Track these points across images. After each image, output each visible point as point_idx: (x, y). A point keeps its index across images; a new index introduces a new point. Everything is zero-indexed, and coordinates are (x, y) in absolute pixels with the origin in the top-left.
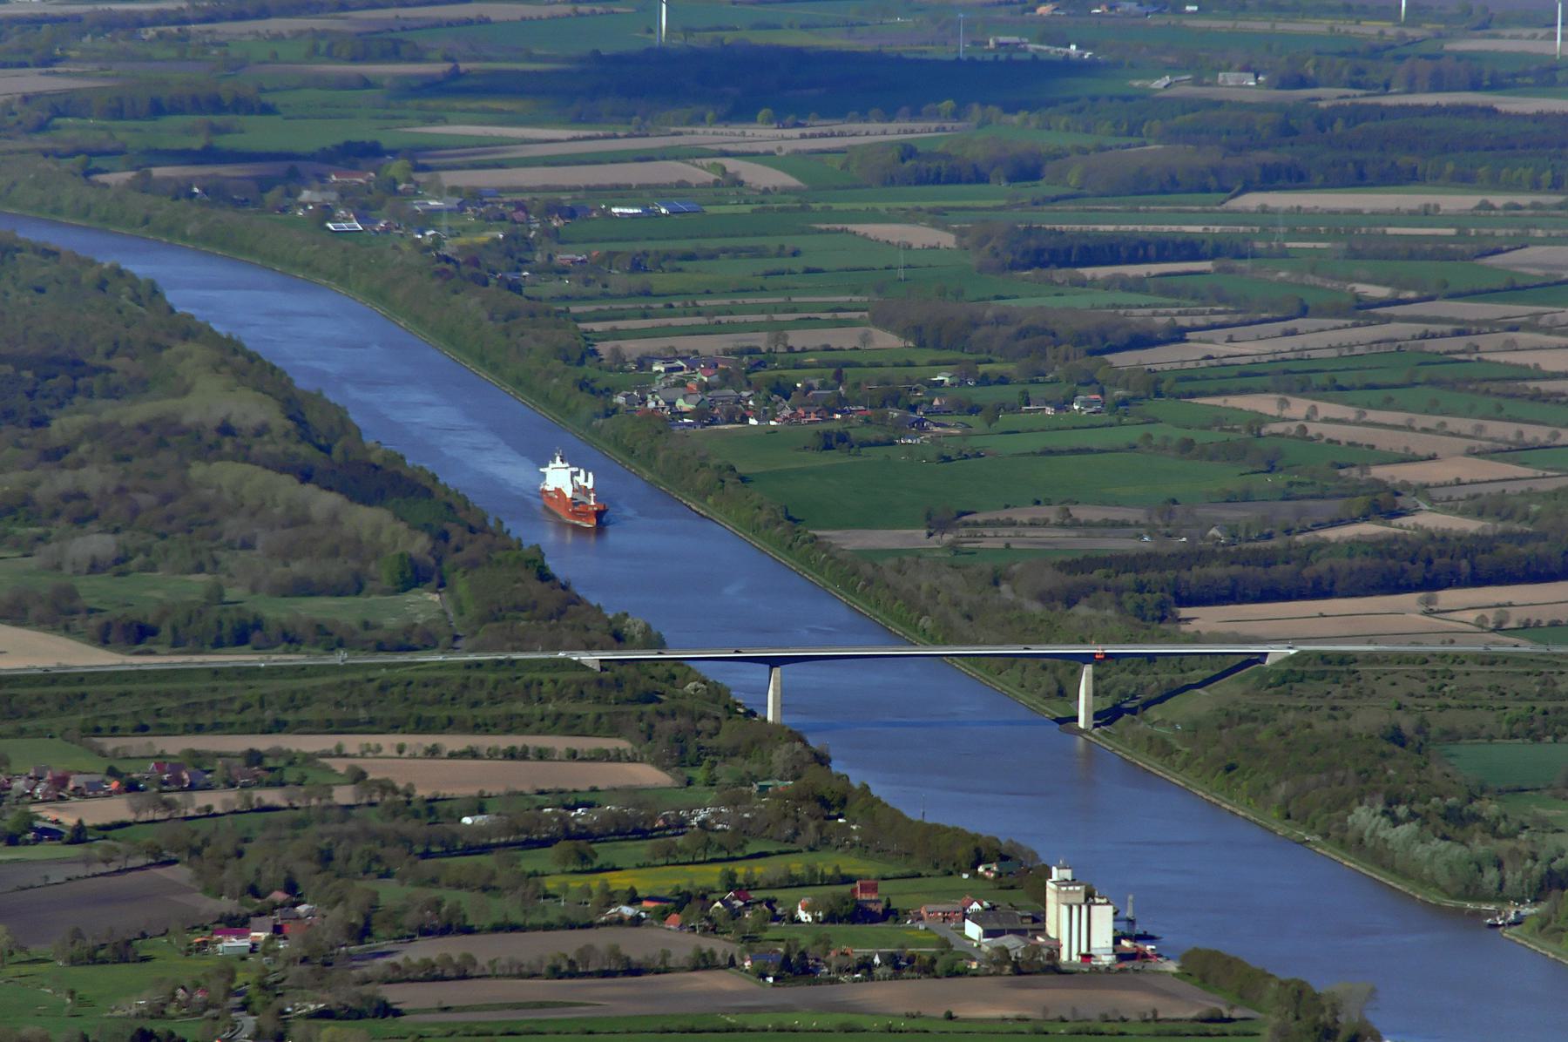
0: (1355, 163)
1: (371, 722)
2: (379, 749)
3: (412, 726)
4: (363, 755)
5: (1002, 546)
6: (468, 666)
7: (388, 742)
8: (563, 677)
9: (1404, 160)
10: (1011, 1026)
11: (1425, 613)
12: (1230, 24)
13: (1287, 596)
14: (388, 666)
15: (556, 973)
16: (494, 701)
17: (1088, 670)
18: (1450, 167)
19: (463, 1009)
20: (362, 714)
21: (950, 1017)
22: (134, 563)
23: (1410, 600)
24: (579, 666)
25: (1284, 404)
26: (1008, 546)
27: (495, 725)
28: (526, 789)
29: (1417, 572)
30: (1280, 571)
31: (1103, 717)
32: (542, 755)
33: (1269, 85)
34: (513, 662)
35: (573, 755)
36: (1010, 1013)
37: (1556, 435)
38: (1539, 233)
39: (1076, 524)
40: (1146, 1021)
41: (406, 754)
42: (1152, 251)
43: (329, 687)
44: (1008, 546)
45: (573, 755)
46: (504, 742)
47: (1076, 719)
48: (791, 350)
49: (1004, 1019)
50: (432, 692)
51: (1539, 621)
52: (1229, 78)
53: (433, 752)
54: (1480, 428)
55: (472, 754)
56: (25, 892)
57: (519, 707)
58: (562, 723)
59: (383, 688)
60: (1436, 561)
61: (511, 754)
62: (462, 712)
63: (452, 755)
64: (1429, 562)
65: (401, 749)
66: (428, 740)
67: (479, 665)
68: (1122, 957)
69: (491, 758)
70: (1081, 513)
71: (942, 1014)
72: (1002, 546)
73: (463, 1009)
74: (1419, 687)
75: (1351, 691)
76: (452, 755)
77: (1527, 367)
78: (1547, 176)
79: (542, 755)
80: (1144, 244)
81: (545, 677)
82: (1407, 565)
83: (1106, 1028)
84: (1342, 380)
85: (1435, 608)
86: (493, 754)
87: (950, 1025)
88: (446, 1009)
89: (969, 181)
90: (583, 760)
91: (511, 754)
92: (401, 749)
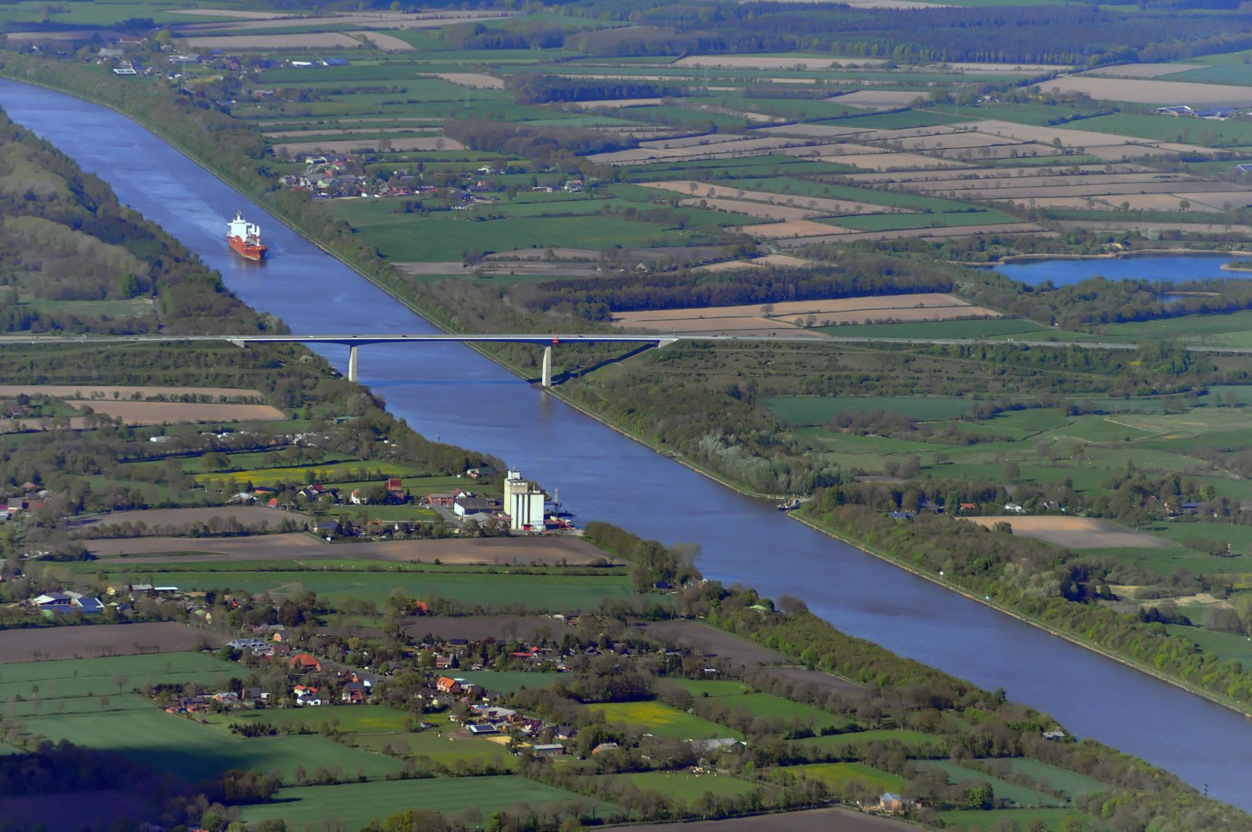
1: (100, 378)
2: (103, 395)
3: (125, 381)
4: (93, 399)
5: (509, 273)
6: (162, 344)
7: (108, 391)
9: (787, 37)
10: (475, 569)
11: (766, 317)
15: (196, 534)
19: (135, 556)
20: (95, 373)
21: (438, 563)
23: (757, 308)
24: (231, 344)
25: (694, 187)
26: (512, 273)
27: (177, 381)
28: (193, 420)
29: (762, 291)
31: (558, 379)
32: (205, 399)
34: (190, 342)
35: (224, 400)
36: (475, 561)
37: (860, 208)
38: (867, 83)
40: (560, 566)
41: (119, 398)
42: (625, 92)
43: (74, 357)
44: (512, 273)
45: (224, 400)
46: (181, 391)
47: (541, 380)
48: (393, 151)
49: (471, 565)
50: (138, 360)
51: (835, 323)
53: (137, 397)
54: (813, 203)
55: (161, 398)
57: (193, 370)
59: (108, 357)
61: (186, 399)
63: (149, 399)
65: (116, 395)
66: (134, 390)
67: (168, 343)
68: (549, 527)
69: (173, 401)
70: (559, 253)
71: (433, 561)
72: (509, 273)
73: (135, 556)
74: (754, 363)
75: (710, 364)
76: (149, 399)
77: (848, 165)
78: (875, 48)
79: (205, 399)
80: (620, 87)
81: (210, 351)
85: (772, 314)
86: (174, 399)
88: (125, 556)
90: (231, 403)
91: (186, 399)
92: (116, 395)
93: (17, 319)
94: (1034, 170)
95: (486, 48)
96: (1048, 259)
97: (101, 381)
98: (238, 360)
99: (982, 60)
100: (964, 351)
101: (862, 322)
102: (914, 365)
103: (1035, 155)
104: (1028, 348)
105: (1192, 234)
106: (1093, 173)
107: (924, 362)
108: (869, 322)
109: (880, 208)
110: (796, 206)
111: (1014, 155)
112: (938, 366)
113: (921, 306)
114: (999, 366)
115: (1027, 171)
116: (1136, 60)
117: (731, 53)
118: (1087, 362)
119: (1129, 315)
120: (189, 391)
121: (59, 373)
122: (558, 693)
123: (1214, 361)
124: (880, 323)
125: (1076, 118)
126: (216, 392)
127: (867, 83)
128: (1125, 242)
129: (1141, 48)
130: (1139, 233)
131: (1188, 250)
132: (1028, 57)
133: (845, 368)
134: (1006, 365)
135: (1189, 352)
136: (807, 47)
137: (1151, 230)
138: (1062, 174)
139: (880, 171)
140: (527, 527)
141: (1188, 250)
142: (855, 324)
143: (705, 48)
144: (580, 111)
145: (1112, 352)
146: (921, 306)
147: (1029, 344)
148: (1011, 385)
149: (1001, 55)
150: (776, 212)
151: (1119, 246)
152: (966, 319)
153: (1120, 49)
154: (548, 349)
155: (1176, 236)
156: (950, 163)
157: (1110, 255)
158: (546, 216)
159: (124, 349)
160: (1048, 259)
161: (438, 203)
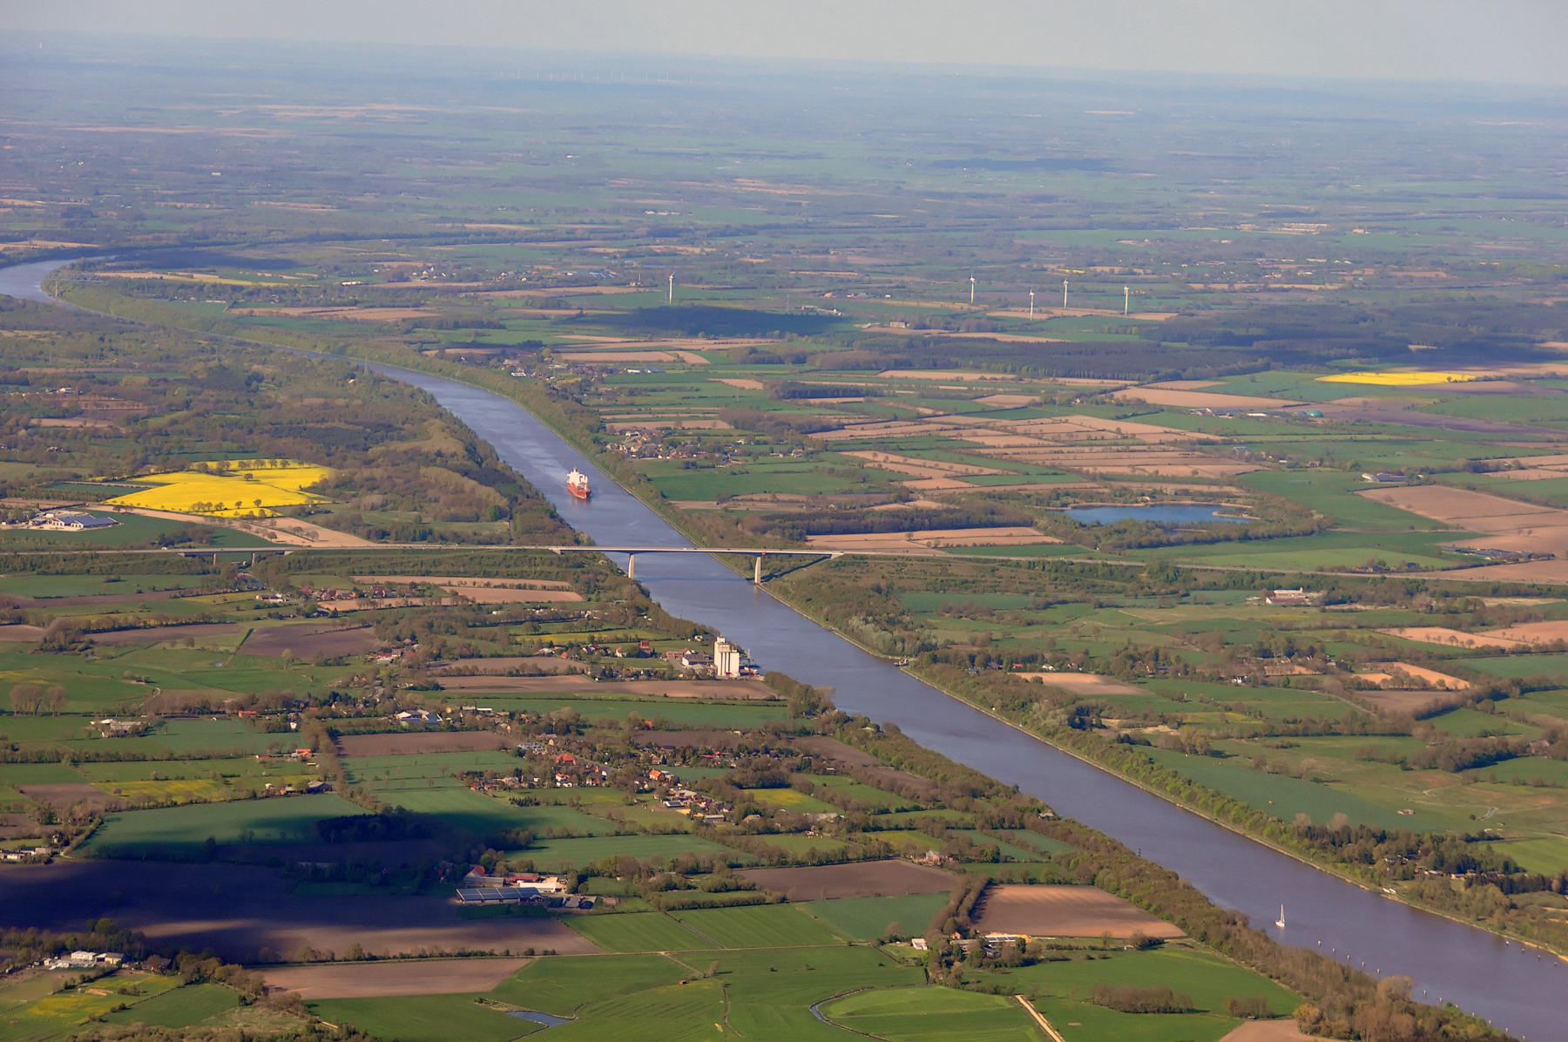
1: (465, 572)
8: (544, 556)
9: (954, 359)
10: (689, 700)
17: (759, 559)
19: (469, 688)
21: (665, 696)
24: (552, 552)
29: (907, 524)
31: (765, 579)
32: (532, 588)
35: (544, 588)
36: (690, 695)
38: (1001, 390)
42: (841, 393)
43: (449, 558)
45: (544, 588)
46: (516, 582)
48: (683, 428)
52: (895, 324)
53: (488, 585)
54: (951, 467)
55: (504, 586)
57: (526, 568)
58: (543, 575)
61: (519, 587)
63: (495, 587)
66: (486, 580)
67: (511, 551)
68: (742, 674)
70: (780, 497)
73: (469, 688)
74: (893, 570)
76: (495, 587)
78: (1009, 368)
79: (532, 588)
81: (537, 556)
87: (665, 699)
91: (519, 587)
92: (474, 583)
93: (418, 534)
95: (756, 363)
97: (466, 574)
100: (1031, 565)
101: (970, 545)
102: (997, 573)
103: (1103, 438)
104: (1072, 564)
105: (1196, 492)
107: (1003, 571)
108: (975, 545)
109: (995, 471)
111: (1089, 438)
113: (1011, 535)
114: (1053, 575)
115: (1095, 449)
118: (1111, 573)
120: (522, 582)
123: (1194, 574)
124: (982, 546)
125: (1134, 415)
127: (1001, 390)
129: (1184, 370)
130: (1161, 491)
133: (953, 575)
137: (1170, 489)
142: (966, 546)
147: (1074, 561)
148: (1060, 588)
149: (1091, 373)
153: (1170, 371)
155: (1186, 493)
156: (1046, 443)
159: (483, 554)
160: (1101, 506)
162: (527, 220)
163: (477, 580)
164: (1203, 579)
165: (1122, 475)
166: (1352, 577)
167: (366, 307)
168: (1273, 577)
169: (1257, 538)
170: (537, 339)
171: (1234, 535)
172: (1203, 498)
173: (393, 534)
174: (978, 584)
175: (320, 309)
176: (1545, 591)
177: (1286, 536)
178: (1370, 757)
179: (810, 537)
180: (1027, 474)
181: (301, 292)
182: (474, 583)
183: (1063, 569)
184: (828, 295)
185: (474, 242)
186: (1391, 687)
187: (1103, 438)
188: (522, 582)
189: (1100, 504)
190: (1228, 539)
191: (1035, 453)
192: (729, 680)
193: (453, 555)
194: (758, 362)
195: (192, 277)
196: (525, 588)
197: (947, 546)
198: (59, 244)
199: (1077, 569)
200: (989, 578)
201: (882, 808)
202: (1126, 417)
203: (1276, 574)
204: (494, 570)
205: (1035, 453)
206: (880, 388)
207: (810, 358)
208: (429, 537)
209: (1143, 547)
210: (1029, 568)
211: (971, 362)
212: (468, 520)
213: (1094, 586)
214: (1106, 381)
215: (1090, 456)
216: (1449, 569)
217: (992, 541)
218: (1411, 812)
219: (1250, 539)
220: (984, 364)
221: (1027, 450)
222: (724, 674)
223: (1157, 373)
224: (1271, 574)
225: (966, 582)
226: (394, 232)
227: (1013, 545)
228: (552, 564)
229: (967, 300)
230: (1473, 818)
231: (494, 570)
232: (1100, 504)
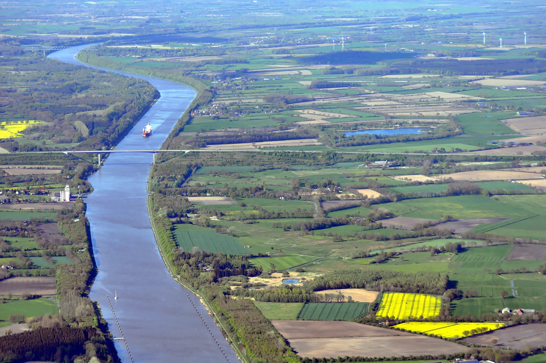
0: (409, 70)
1: (22, 163)
6: (44, 154)
8: (58, 155)
9: (418, 69)
12: (465, 46)
13: (234, 143)
14: (30, 154)
16: (45, 159)
17: (99, 155)
18: (426, 70)
20: (21, 162)
21: (20, 209)
22: (40, 138)
24: (64, 154)
25: (304, 111)
29: (258, 139)
30: (232, 139)
32: (43, 168)
33: (436, 56)
35: (49, 168)
36: (30, 209)
37: (340, 116)
38: (422, 82)
39: (228, 131)
42: (341, 85)
43: (18, 157)
45: (49, 168)
46: (37, 166)
48: (242, 103)
52: (429, 55)
53: (25, 168)
54: (329, 115)
55: (31, 168)
56: (441, 185)
57: (50, 161)
59: (27, 158)
60: (263, 137)
61: (38, 168)
62: (39, 161)
63: (28, 169)
64: (261, 137)
66: (24, 166)
67: (46, 153)
68: (70, 200)
74: (209, 157)
75: (196, 158)
76: (28, 169)
78: (441, 72)
79: (43, 168)
80: (339, 84)
81: (56, 155)
82: (256, 137)
83: (45, 211)
84: (324, 107)
87: (21, 211)
89: (341, 74)
91: (38, 168)
92: (19, 167)
93: (30, 148)
94: (414, 105)
95: (331, 74)
96: (375, 130)
98: (63, 158)
99: (470, 75)
101: (276, 147)
102: (255, 157)
103: (427, 101)
104: (289, 153)
105: (422, 122)
106: (433, 106)
108: (278, 147)
110: (310, 114)
111: (420, 101)
112: (261, 158)
113: (302, 142)
114: (279, 157)
115: (412, 106)
116: (518, 74)
117: (400, 74)
118: (305, 156)
119: (356, 144)
120: (39, 166)
121: (12, 162)
122: (306, 226)
124: (281, 147)
125: (463, 90)
126: (47, 167)
127: (422, 82)
128: (401, 124)
129: (521, 70)
130: (407, 122)
131: (419, 127)
132: (483, 73)
134: (281, 157)
135: (337, 153)
136: (424, 72)
137: (410, 121)
138: (423, 106)
139: (372, 106)
140: (65, 200)
141: (419, 127)
142: (273, 147)
143: (392, 73)
144: (320, 91)
145: (313, 154)
146: (302, 142)
147: (290, 151)
148: (280, 163)
149: (476, 73)
150: (313, 117)
151: (398, 125)
152: (308, 145)
153: (512, 71)
154: (99, 155)
155: (418, 122)
157: (393, 128)
158: (251, 119)
159: (31, 155)
160: (375, 130)
161: (223, 116)
162: (359, 16)
163: (20, 166)
164: (346, 157)
165: (406, 116)
166: (414, 155)
167: (198, 56)
168: (378, 156)
169: (414, 140)
170: (103, 70)
171: (401, 139)
172: (423, 125)
173: (20, 149)
174: (243, 162)
175: (174, 58)
176: (499, 158)
177: (431, 139)
178: (277, 226)
179: (208, 146)
180: (361, 117)
181: (181, 51)
182: (19, 167)
183: (284, 155)
184: (422, 43)
185: (316, 26)
186: (345, 199)
187: (427, 101)
188: (39, 166)
189: (374, 128)
190: (398, 141)
191: (383, 108)
192: (65, 203)
193: (19, 156)
194: (334, 73)
195: (151, 46)
196: (40, 168)
197: (265, 148)
198: (127, 34)
199: (290, 154)
200: (250, 159)
201: (16, 249)
202: (458, 91)
203: (379, 155)
204: (35, 162)
205: (383, 108)
206: (360, 83)
207: (354, 71)
208: (35, 149)
209: (355, 146)
210: (269, 155)
211: (426, 70)
212: (67, 142)
213: (295, 162)
214: (478, 76)
215: (410, 108)
216: (473, 151)
217: (286, 145)
218: (248, 247)
219: (410, 141)
220: (431, 71)
221: (379, 107)
222: (63, 200)
223: (505, 72)
224: (377, 155)
225: (239, 161)
226: (283, 24)
227: (295, 146)
228: (61, 158)
229: (482, 43)
230: (273, 248)
231: (35, 162)
232: (374, 128)
